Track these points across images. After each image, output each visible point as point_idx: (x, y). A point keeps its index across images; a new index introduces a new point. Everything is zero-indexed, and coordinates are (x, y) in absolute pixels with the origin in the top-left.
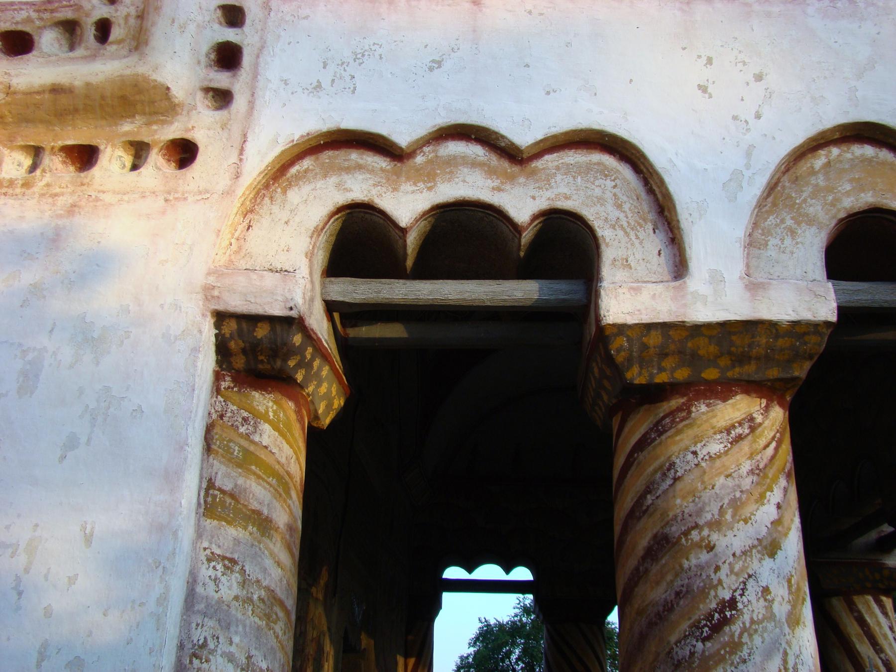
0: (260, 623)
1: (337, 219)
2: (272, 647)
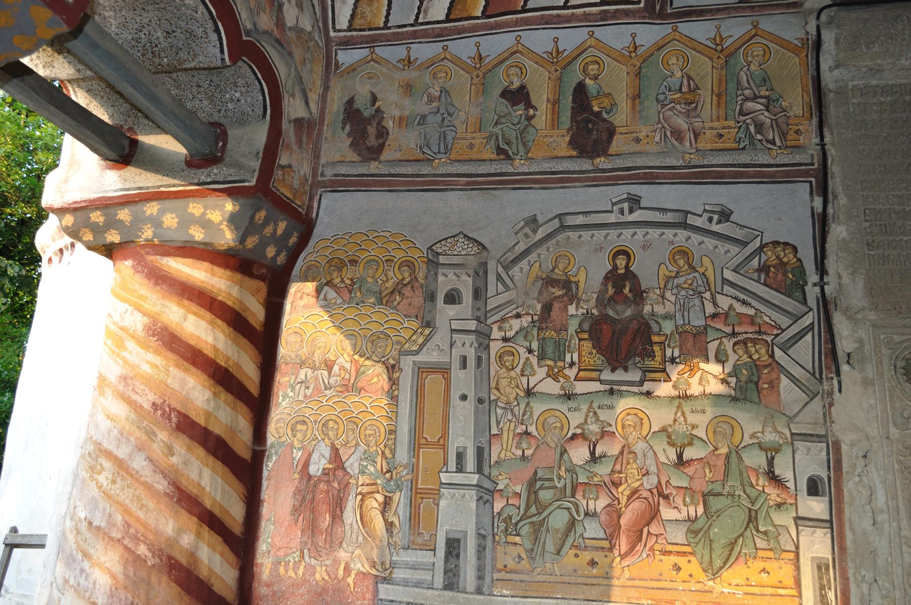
0: (85, 475)
1: (75, 92)
2: (93, 497)
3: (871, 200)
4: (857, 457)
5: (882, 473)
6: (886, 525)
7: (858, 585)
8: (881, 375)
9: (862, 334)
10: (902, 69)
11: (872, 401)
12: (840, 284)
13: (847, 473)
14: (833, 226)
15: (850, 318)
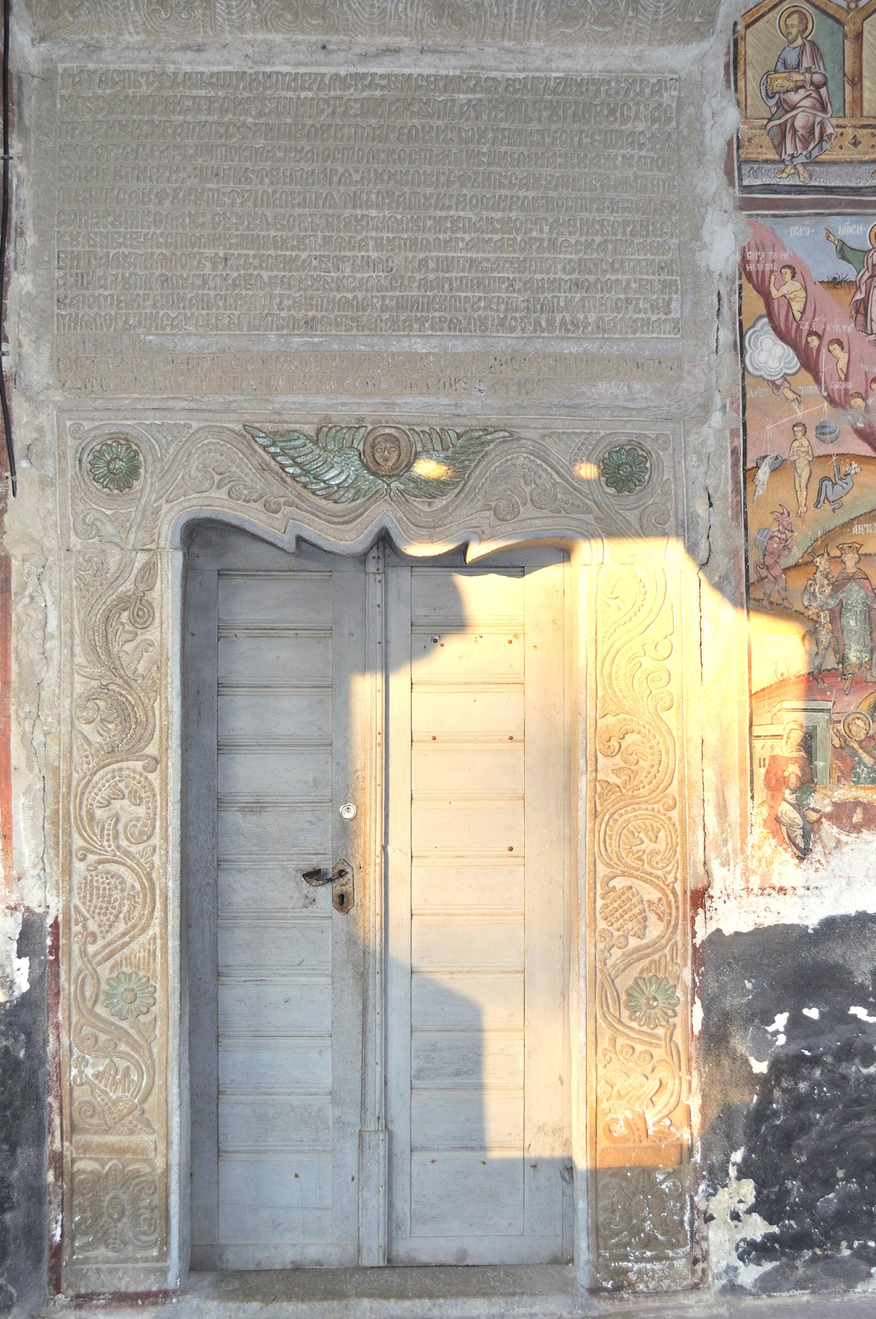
3: (67, 238)
4: (29, 575)
5: (56, 592)
6: (56, 653)
7: (19, 723)
8: (62, 472)
9: (42, 419)
10: (127, 48)
11: (50, 506)
12: (20, 355)
13: (16, 594)
14: (14, 275)
15: (29, 399)
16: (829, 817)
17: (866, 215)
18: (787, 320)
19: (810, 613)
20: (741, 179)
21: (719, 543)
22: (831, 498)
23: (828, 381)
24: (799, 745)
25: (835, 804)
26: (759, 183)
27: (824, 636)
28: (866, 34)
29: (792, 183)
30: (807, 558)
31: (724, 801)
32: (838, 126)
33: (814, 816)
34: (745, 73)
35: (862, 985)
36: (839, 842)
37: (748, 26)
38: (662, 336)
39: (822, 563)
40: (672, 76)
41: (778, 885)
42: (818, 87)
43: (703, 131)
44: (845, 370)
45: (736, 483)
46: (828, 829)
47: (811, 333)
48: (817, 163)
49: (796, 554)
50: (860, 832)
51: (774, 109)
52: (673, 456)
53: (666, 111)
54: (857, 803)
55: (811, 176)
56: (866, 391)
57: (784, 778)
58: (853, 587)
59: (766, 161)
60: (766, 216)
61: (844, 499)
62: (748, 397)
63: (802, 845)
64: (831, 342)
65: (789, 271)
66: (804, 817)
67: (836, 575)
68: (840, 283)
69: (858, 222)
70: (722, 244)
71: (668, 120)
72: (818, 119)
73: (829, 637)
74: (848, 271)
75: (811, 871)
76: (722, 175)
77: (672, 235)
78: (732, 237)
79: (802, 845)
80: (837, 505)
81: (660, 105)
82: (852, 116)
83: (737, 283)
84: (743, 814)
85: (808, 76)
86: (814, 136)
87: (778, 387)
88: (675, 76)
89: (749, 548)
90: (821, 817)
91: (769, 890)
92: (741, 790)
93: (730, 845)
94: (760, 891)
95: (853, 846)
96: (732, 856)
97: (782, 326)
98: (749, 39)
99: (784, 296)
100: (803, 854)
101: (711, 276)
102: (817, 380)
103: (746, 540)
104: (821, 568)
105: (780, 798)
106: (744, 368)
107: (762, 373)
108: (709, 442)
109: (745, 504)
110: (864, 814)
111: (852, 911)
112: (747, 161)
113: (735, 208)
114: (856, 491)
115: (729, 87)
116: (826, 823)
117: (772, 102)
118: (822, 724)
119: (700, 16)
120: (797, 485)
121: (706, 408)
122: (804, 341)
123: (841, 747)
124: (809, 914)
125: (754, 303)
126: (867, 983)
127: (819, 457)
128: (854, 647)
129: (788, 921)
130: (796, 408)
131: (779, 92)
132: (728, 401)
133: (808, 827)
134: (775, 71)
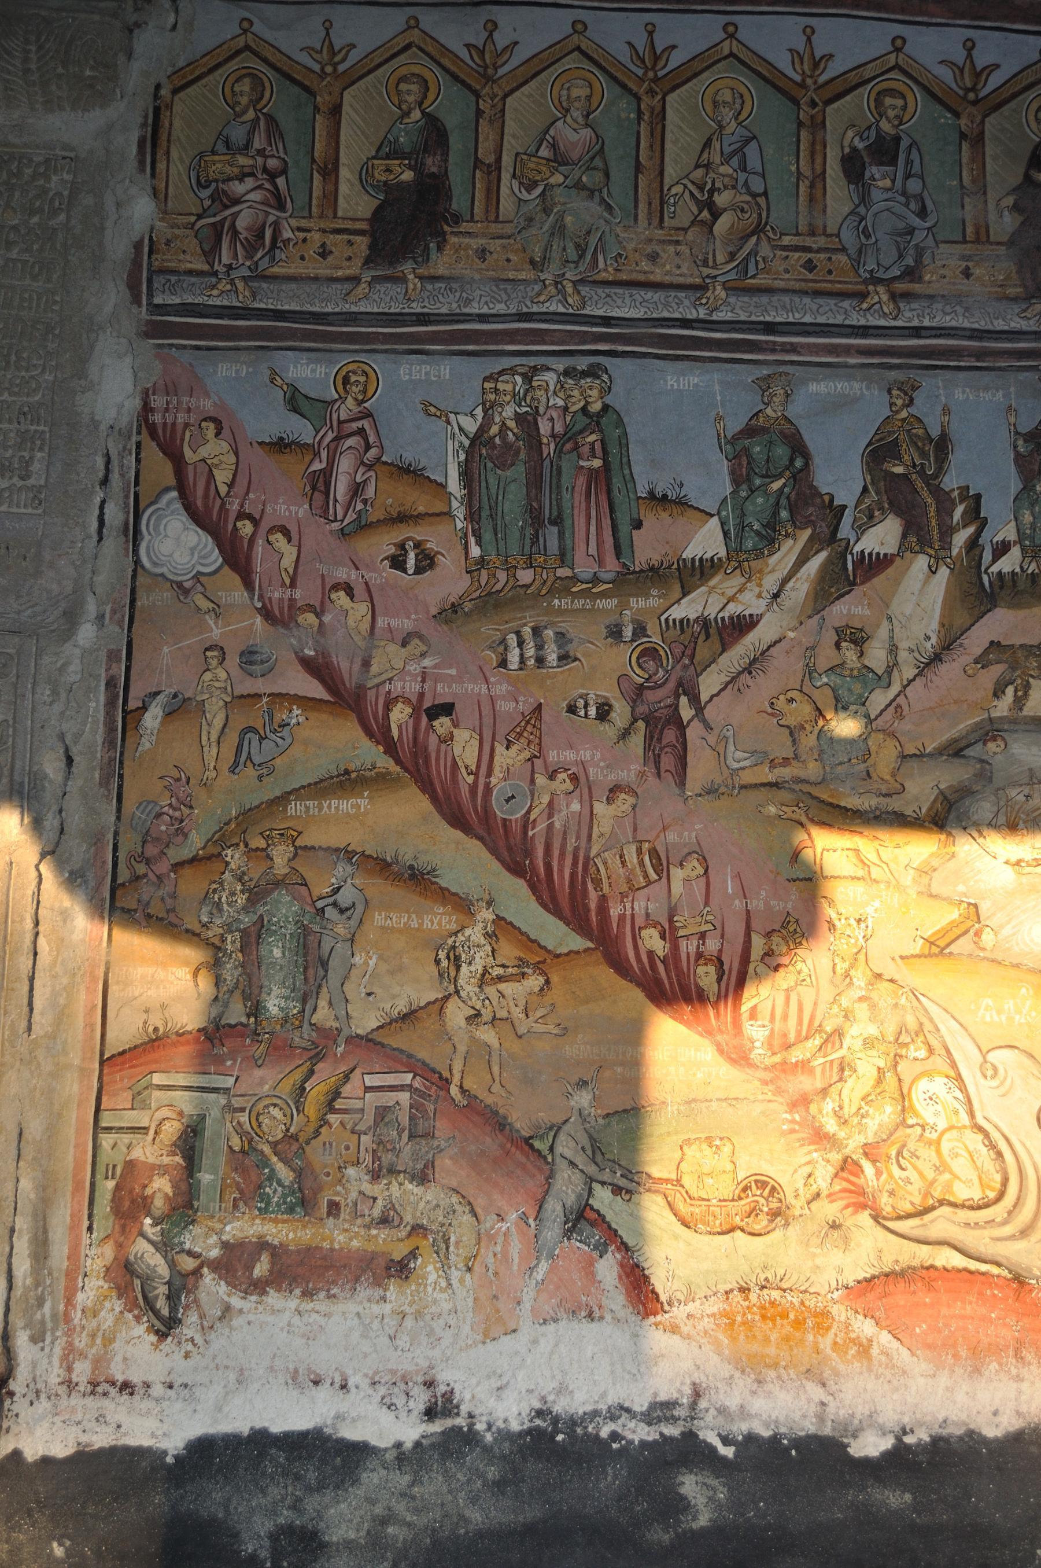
16: (216, 1266)
17: (331, 351)
18: (206, 496)
19: (210, 934)
20: (150, 295)
21: (75, 820)
22: (257, 760)
23: (265, 585)
24: (174, 1144)
25: (225, 1245)
26: (178, 301)
27: (230, 973)
28: (346, 108)
29: (226, 303)
30: (212, 850)
31: (45, 1231)
32: (300, 229)
33: (188, 1264)
34: (168, 153)
35: (253, 1558)
36: (227, 1308)
37: (175, 91)
38: (15, 510)
39: (234, 857)
40: (66, 154)
41: (120, 1378)
42: (272, 176)
43: (103, 229)
44: (291, 571)
45: (111, 729)
46: (212, 1288)
47: (241, 516)
48: (265, 278)
49: (196, 842)
50: (263, 1293)
51: (207, 203)
52: (15, 686)
53: (52, 200)
54: (262, 1245)
55: (254, 295)
56: (322, 603)
57: (145, 1198)
58: (283, 896)
59: (190, 272)
60: (185, 347)
61: (278, 762)
62: (139, 603)
63: (165, 1312)
64: (271, 530)
65: (212, 426)
66: (172, 1265)
67: (256, 876)
68: (286, 446)
69: (318, 361)
70: (114, 387)
71: (54, 212)
72: (271, 219)
73: (236, 974)
74: (302, 430)
75: (178, 1356)
76: (123, 287)
77: (44, 368)
78: (129, 374)
79: (165, 1312)
80: (266, 769)
81: (45, 191)
82: (321, 217)
83: (134, 439)
84: (74, 1256)
85: (260, 160)
86: (263, 241)
87: (186, 592)
88: (72, 155)
89: (122, 829)
90: (201, 1266)
91: (105, 1387)
92: (72, 1216)
93: (48, 1305)
94: (89, 1388)
95: (251, 1317)
96: (49, 1325)
97: (199, 503)
98: (177, 107)
99: (203, 460)
100: (166, 1327)
101: (96, 427)
102: (248, 584)
103: (118, 818)
104: (233, 866)
105: (135, 1231)
106: (137, 562)
107: (164, 570)
108: (72, 668)
109: (121, 763)
110: (273, 1264)
111: (243, 1427)
112: (162, 271)
113: (138, 334)
114: (296, 751)
115: (142, 170)
116: (208, 1277)
117: (205, 193)
118: (215, 1113)
119: (92, 68)
120: (204, 738)
121: (72, 618)
122: (230, 527)
123: (242, 1151)
124: (161, 1429)
125: (158, 467)
126: (263, 1554)
127: (242, 696)
128: (276, 990)
129: (132, 1442)
130: (211, 623)
131: (216, 181)
132: (108, 609)
133: (178, 1282)
134: (213, 152)
